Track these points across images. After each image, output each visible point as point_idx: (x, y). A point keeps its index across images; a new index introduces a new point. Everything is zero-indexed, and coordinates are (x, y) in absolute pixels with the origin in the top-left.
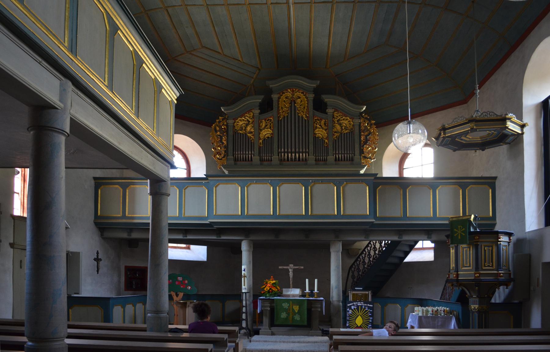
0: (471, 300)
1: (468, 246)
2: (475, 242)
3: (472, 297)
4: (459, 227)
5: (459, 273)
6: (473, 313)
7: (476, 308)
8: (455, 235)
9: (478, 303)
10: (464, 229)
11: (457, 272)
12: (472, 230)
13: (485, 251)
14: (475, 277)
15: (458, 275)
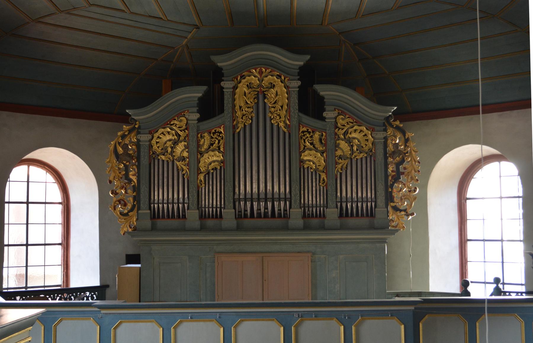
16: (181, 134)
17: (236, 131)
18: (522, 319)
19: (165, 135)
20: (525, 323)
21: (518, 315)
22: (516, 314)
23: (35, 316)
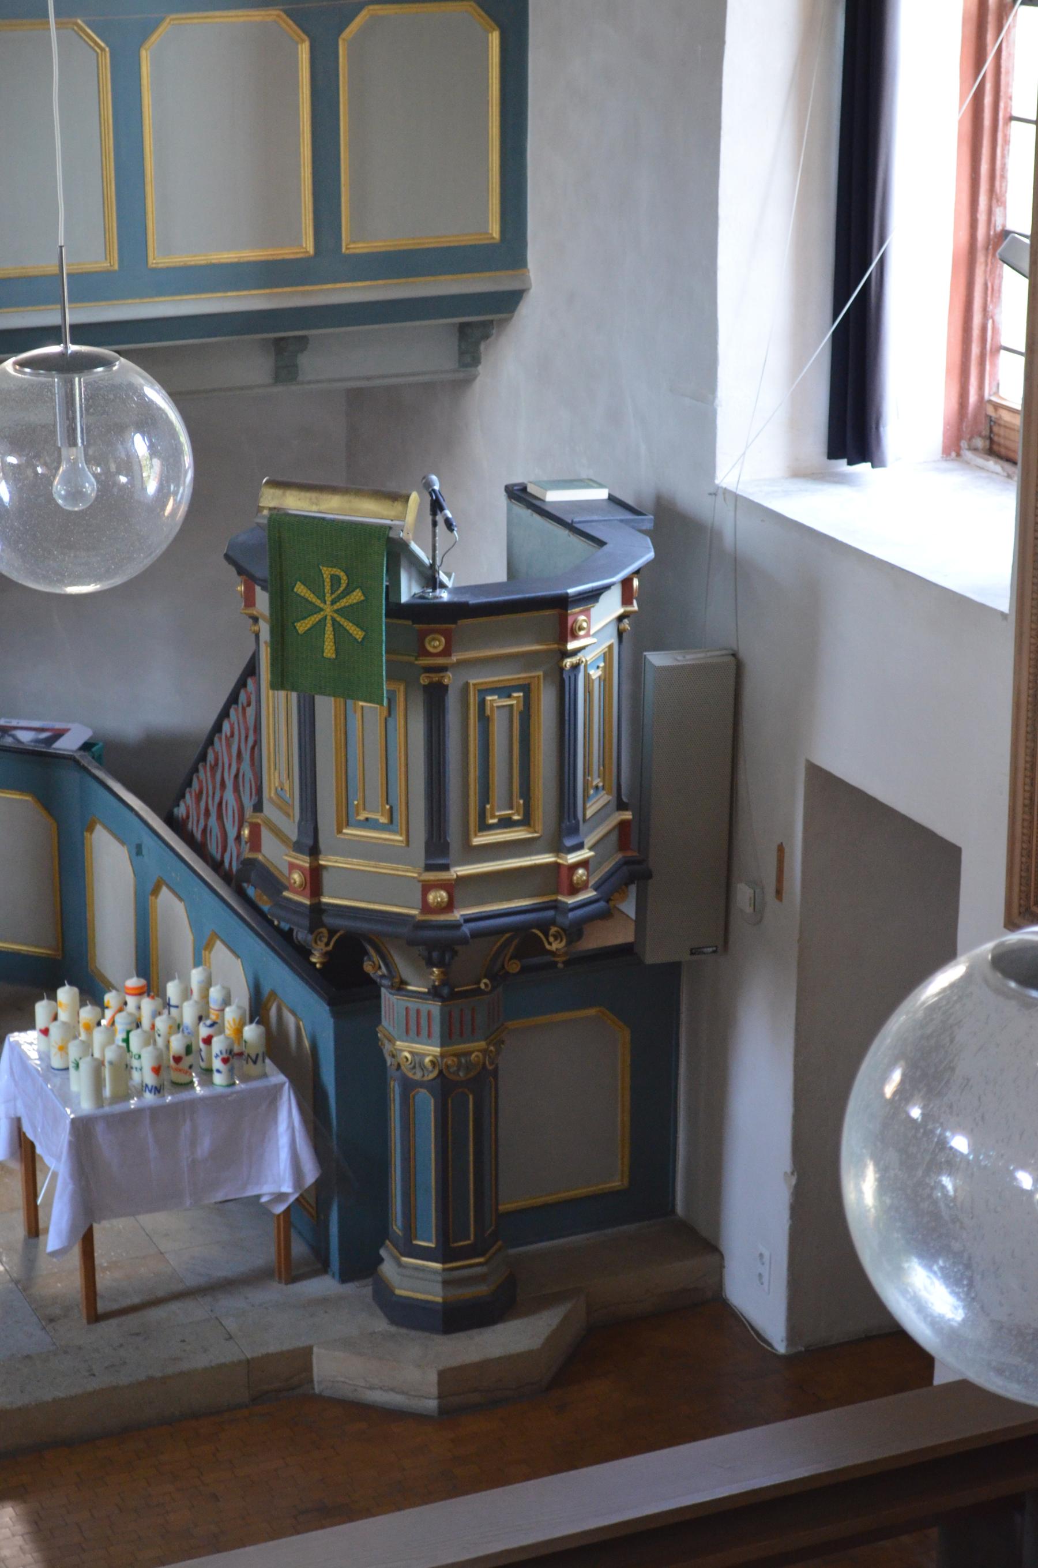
0: (391, 1002)
1: (404, 986)
2: (429, 669)
3: (400, 987)
4: (327, 572)
5: (325, 900)
6: (408, 1086)
7: (427, 1060)
8: (302, 627)
9: (436, 1028)
10: (357, 596)
11: (314, 851)
12: (408, 590)
13: (485, 720)
14: (426, 908)
15: (315, 877)
16: (275, 784)
17: (566, 946)
18: (103, 40)
19: (970, 1258)
20: (111, 54)
21: (84, 21)
22: (79, 21)
23: (643, 679)
